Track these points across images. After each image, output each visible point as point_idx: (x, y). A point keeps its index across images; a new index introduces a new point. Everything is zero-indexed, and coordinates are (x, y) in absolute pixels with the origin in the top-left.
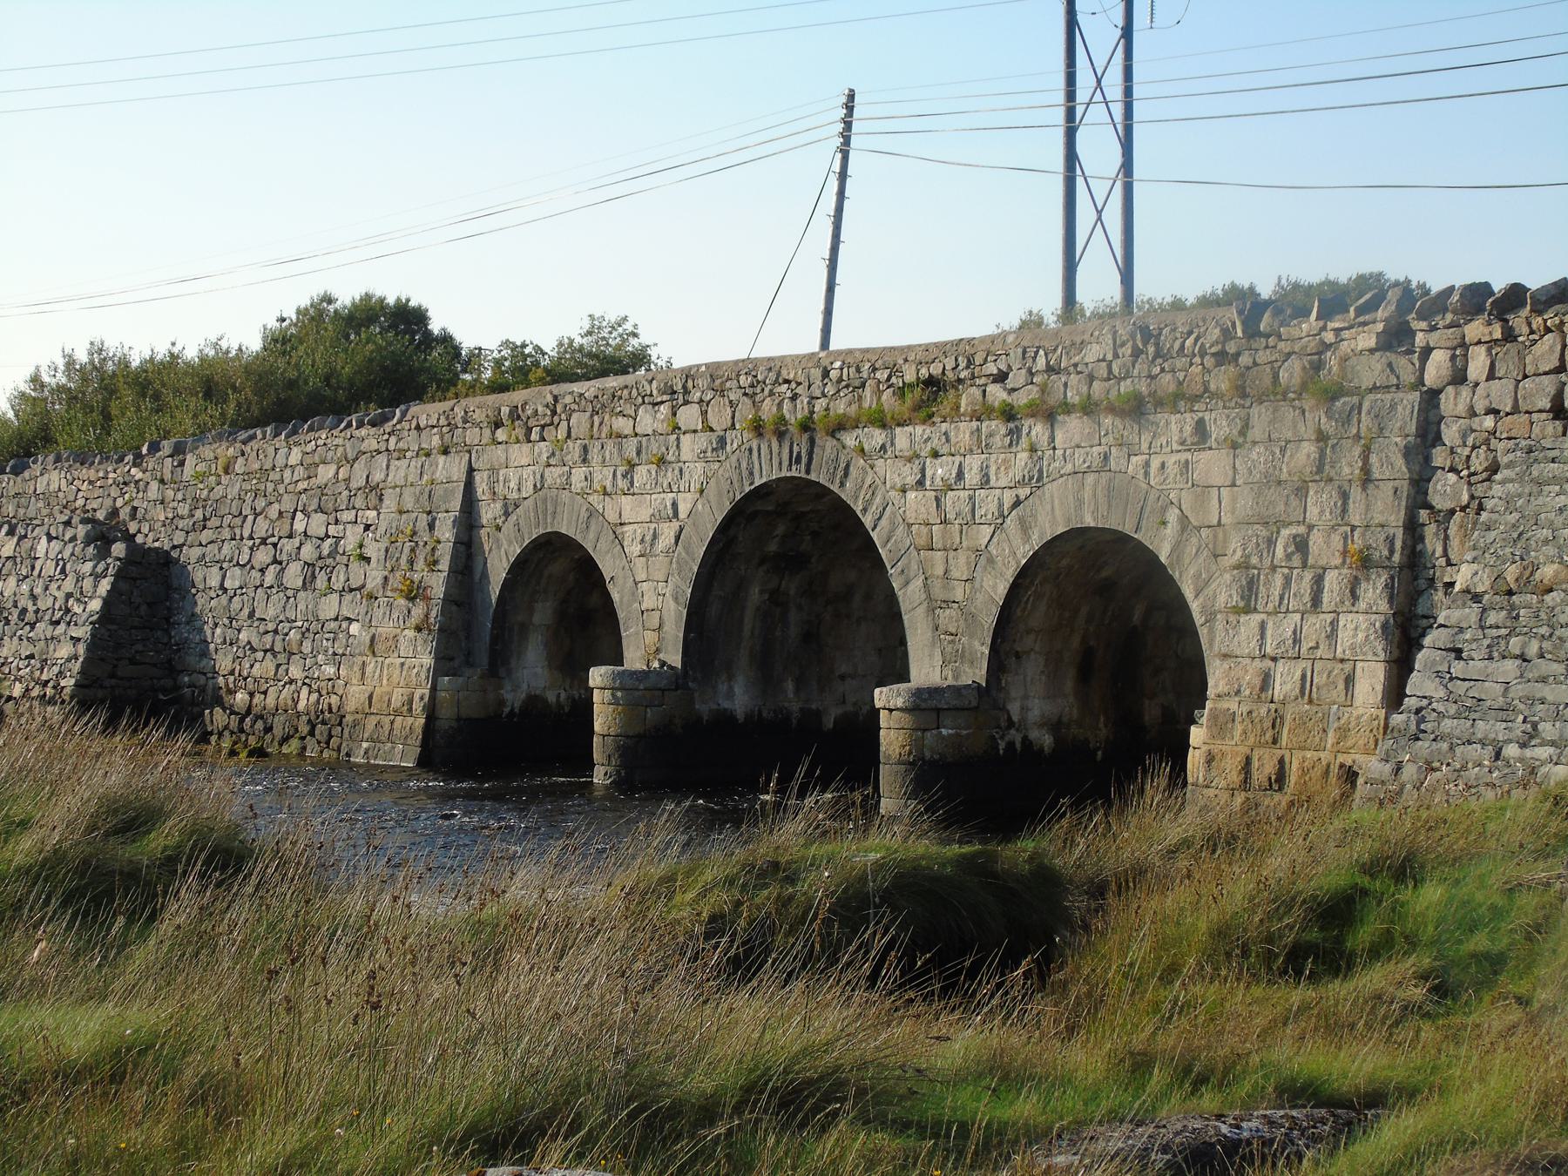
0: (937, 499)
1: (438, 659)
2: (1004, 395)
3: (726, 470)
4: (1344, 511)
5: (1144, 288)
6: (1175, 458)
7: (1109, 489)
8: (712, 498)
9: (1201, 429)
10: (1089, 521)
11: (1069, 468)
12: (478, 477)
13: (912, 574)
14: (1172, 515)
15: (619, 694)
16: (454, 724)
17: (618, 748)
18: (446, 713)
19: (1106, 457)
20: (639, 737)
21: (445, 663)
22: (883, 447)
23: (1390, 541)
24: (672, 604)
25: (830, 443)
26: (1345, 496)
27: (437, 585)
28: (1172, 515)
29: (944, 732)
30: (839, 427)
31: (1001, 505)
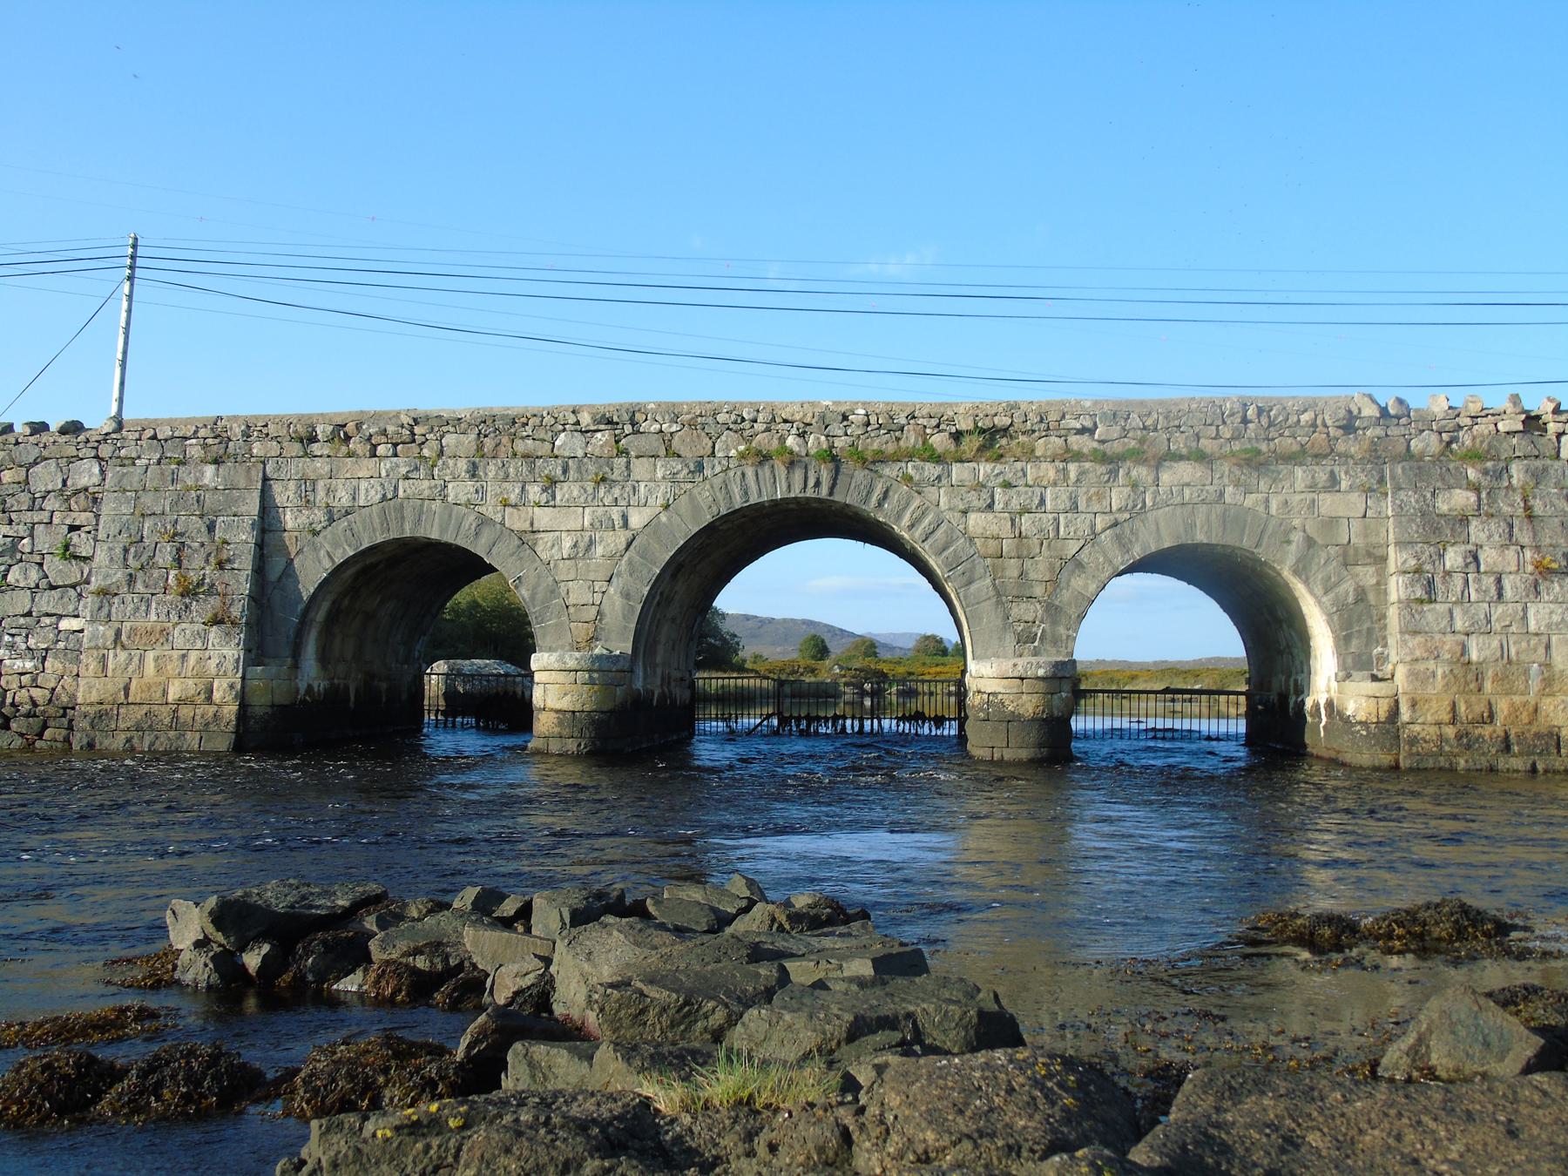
0: (1013, 521)
1: (248, 651)
2: (1095, 445)
3: (704, 494)
4: (1511, 536)
8: (682, 511)
9: (1333, 480)
12: (277, 488)
13: (977, 575)
14: (1297, 537)
15: (595, 675)
16: (269, 710)
17: (593, 722)
18: (260, 702)
20: (611, 712)
22: (939, 478)
24: (618, 601)
26: (1511, 526)
27: (241, 583)
28: (1297, 537)
29: (886, 723)
30: (881, 458)
31: (1093, 526)
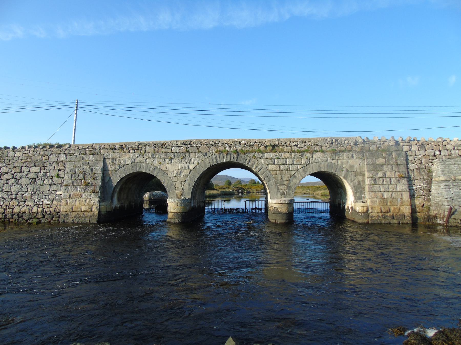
1: (100, 199)
3: (207, 161)
5: (75, 144)
6: (344, 160)
7: (328, 165)
9: (353, 156)
10: (322, 170)
11: (317, 161)
12: (107, 160)
14: (344, 170)
19: (327, 160)
20: (109, 212)
21: (102, 199)
23: (405, 173)
24: (187, 186)
25: (244, 156)
27: (99, 183)
28: (344, 170)
